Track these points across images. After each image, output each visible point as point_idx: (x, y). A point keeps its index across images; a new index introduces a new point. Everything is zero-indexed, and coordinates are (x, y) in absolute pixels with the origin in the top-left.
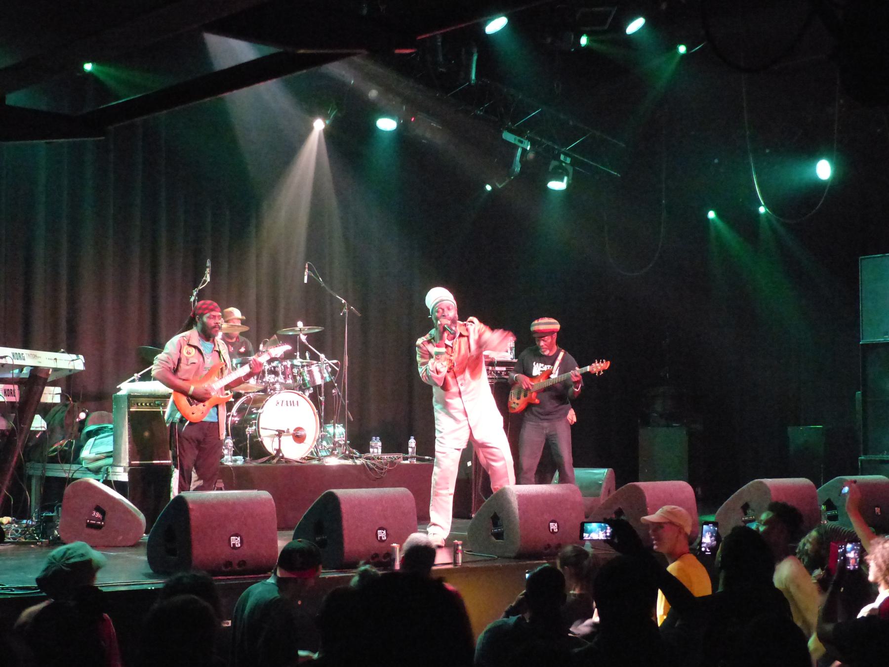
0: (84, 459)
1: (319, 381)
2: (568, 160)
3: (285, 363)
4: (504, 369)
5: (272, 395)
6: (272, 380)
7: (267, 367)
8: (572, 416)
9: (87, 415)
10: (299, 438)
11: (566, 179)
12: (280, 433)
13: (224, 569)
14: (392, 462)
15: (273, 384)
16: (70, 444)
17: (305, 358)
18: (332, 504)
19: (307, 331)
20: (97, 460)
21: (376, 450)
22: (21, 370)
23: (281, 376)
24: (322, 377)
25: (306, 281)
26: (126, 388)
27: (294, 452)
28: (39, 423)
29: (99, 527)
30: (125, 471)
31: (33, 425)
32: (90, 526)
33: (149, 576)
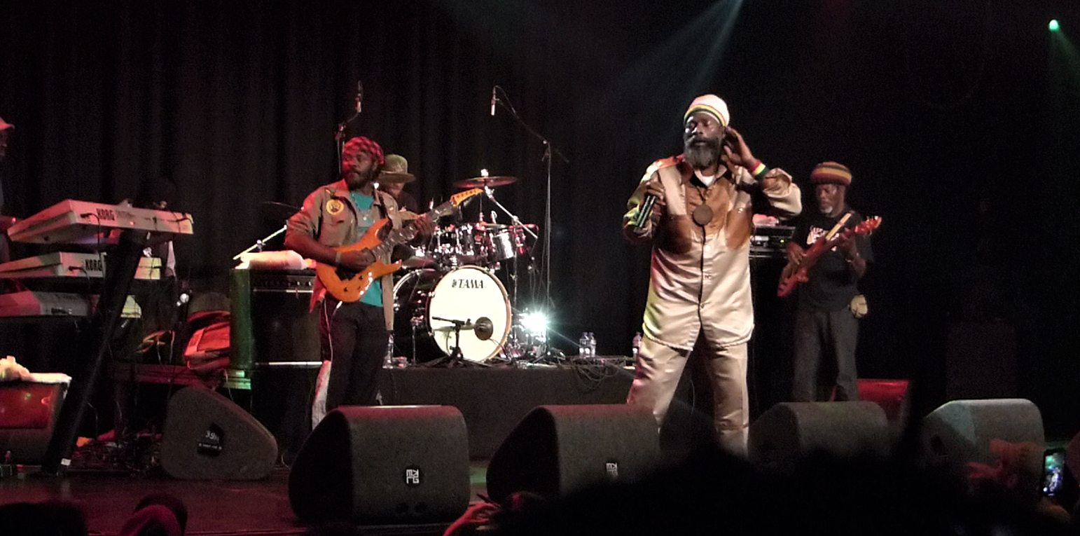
0: (189, 358)
3: (464, 228)
5: (445, 273)
6: (447, 251)
8: (860, 306)
9: (191, 297)
10: (483, 330)
12: (459, 326)
15: (448, 256)
18: (543, 422)
21: (587, 351)
22: (107, 235)
24: (514, 248)
27: (476, 351)
28: (131, 308)
30: (246, 376)
31: (125, 311)
32: (203, 451)
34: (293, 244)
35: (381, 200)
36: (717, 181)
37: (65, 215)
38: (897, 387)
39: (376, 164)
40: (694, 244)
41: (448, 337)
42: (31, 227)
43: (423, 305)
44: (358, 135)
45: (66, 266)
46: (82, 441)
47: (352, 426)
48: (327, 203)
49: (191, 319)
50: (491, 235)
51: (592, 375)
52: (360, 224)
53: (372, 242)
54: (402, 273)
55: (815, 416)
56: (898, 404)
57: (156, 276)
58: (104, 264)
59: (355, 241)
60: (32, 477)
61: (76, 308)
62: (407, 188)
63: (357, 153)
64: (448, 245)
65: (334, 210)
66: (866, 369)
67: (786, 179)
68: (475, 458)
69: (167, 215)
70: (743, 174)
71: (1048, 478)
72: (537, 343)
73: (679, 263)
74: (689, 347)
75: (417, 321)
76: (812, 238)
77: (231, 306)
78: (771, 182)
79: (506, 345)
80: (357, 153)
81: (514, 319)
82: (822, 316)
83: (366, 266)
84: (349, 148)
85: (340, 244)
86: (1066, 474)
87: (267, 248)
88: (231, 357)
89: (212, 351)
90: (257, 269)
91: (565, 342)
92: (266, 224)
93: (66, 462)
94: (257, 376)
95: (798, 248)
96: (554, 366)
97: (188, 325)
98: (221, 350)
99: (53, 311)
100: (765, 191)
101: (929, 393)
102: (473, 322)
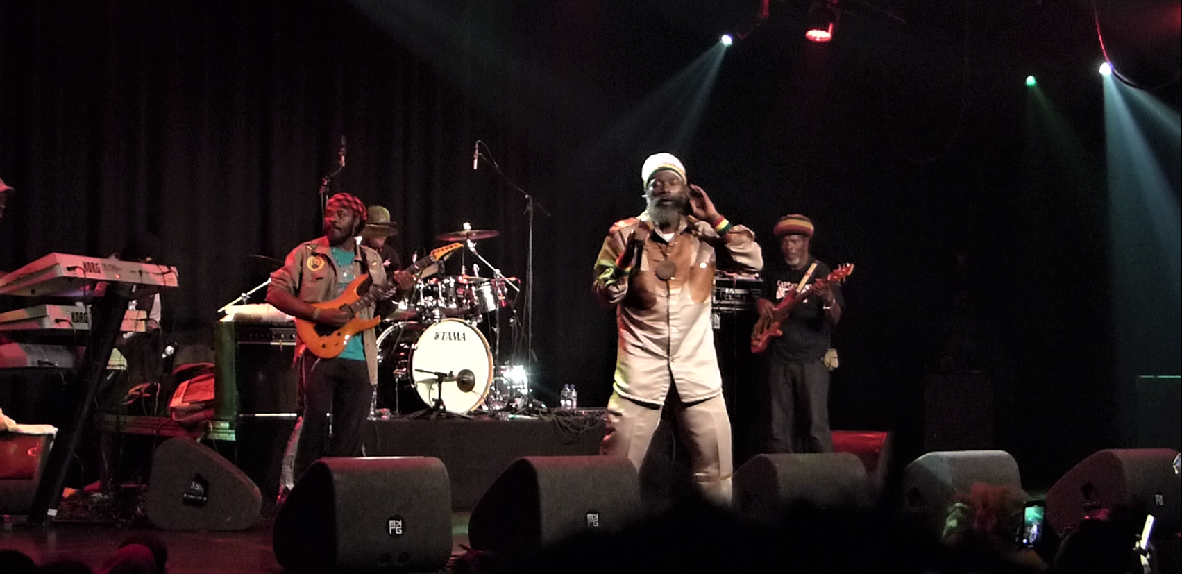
0: (173, 409)
1: (491, 306)
3: (446, 281)
5: (429, 325)
6: (430, 304)
8: (832, 359)
9: (176, 349)
10: (465, 382)
12: (441, 378)
15: (431, 309)
16: (152, 389)
18: (524, 476)
20: (196, 411)
21: (569, 403)
22: (93, 288)
24: (496, 301)
27: (458, 403)
28: (117, 360)
29: (200, 504)
30: (231, 428)
31: (110, 362)
32: (187, 502)
34: (273, 300)
35: (364, 256)
36: (675, 238)
37: (51, 268)
38: (877, 439)
39: (358, 221)
40: (658, 299)
41: (431, 389)
42: (18, 280)
43: (405, 357)
44: (341, 192)
45: (52, 319)
46: (68, 492)
47: (336, 477)
48: (307, 260)
49: (176, 371)
50: (473, 288)
51: (573, 427)
52: (340, 281)
53: (352, 297)
54: (385, 326)
55: (792, 467)
56: (876, 455)
57: (142, 328)
58: (89, 316)
59: (335, 297)
60: (18, 527)
61: (62, 360)
62: (389, 241)
63: (339, 210)
64: (431, 298)
65: (315, 266)
66: (837, 422)
67: (750, 236)
68: (457, 508)
69: (152, 268)
70: (705, 227)
71: (1028, 529)
72: (520, 395)
73: (645, 320)
74: (661, 402)
75: (400, 373)
76: (781, 293)
77: (216, 359)
78: (733, 236)
79: (488, 397)
80: (339, 210)
81: (497, 372)
82: (793, 366)
83: (343, 324)
84: (330, 204)
85: (319, 300)
86: (1045, 525)
87: (250, 302)
88: (215, 408)
89: (197, 402)
90: (244, 326)
91: (545, 390)
92: (248, 280)
93: (52, 513)
94: (242, 428)
95: (769, 304)
96: (535, 418)
97: (173, 377)
98: (206, 402)
99: (40, 363)
100: (728, 246)
101: (908, 445)
102: (456, 374)
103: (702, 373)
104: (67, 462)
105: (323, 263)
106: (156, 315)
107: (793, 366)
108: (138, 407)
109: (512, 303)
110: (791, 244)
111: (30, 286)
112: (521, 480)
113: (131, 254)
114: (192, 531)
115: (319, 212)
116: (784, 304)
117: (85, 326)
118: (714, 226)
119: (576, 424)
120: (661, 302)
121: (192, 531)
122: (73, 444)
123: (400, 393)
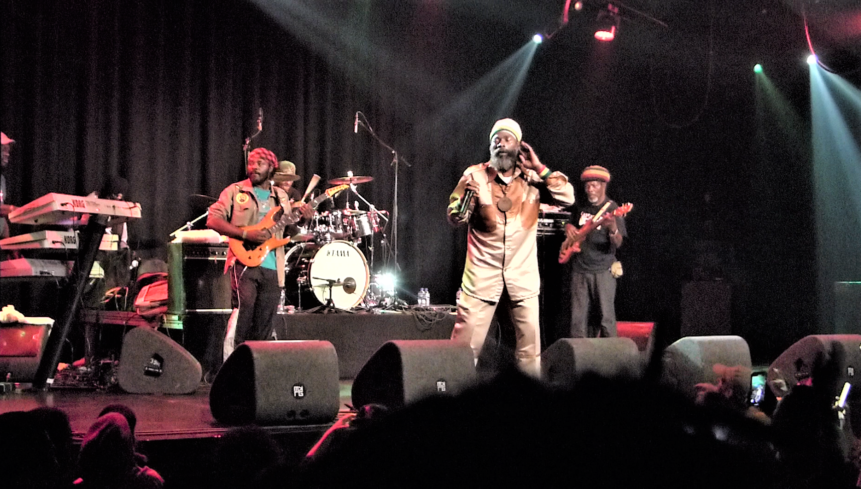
0: (138, 307)
1: (368, 232)
2: (616, 10)
3: (335, 213)
4: (552, 221)
6: (323, 230)
7: (317, 216)
8: (617, 269)
9: (140, 263)
10: (349, 288)
11: (613, 29)
12: (331, 283)
13: (288, 419)
14: (440, 314)
15: (324, 234)
16: (122, 292)
17: (354, 208)
19: (356, 181)
20: (152, 308)
21: (424, 301)
22: (79, 219)
23: (333, 226)
24: (371, 228)
25: (356, 131)
26: (180, 236)
27: (344, 302)
28: (97, 271)
29: (156, 375)
30: (179, 319)
32: (148, 373)
33: (213, 425)
35: (276, 193)
38: (646, 327)
40: (498, 226)
42: (25, 213)
43: (306, 268)
46: (62, 366)
47: (255, 355)
48: (235, 195)
49: (141, 278)
52: (260, 210)
53: (270, 223)
54: (290, 245)
55: (586, 349)
56: (646, 340)
57: (115, 247)
58: (77, 239)
59: (257, 223)
61: (57, 271)
63: (259, 160)
64: (324, 226)
65: (242, 200)
66: (622, 314)
67: (565, 180)
68: (343, 378)
70: (533, 175)
71: (754, 392)
72: (388, 296)
74: (497, 300)
75: (301, 280)
78: (553, 181)
80: (259, 160)
84: (252, 156)
87: (193, 228)
88: (168, 304)
90: (189, 247)
91: (408, 296)
92: (196, 212)
93: (50, 381)
94: (190, 320)
95: (572, 228)
97: (138, 284)
99: (42, 273)
100: (549, 187)
101: (668, 332)
102: (342, 281)
103: (527, 282)
104: (60, 346)
105: (247, 198)
106: (125, 238)
107: (590, 276)
108: (111, 305)
109: (383, 229)
110: (592, 188)
111: (34, 217)
112: (389, 359)
113: (106, 193)
114: (149, 394)
115: (243, 162)
116: (585, 229)
117: (74, 246)
118: (538, 173)
119: (429, 316)
120: (500, 228)
121: (149, 394)
122: (66, 328)
123: (303, 297)
